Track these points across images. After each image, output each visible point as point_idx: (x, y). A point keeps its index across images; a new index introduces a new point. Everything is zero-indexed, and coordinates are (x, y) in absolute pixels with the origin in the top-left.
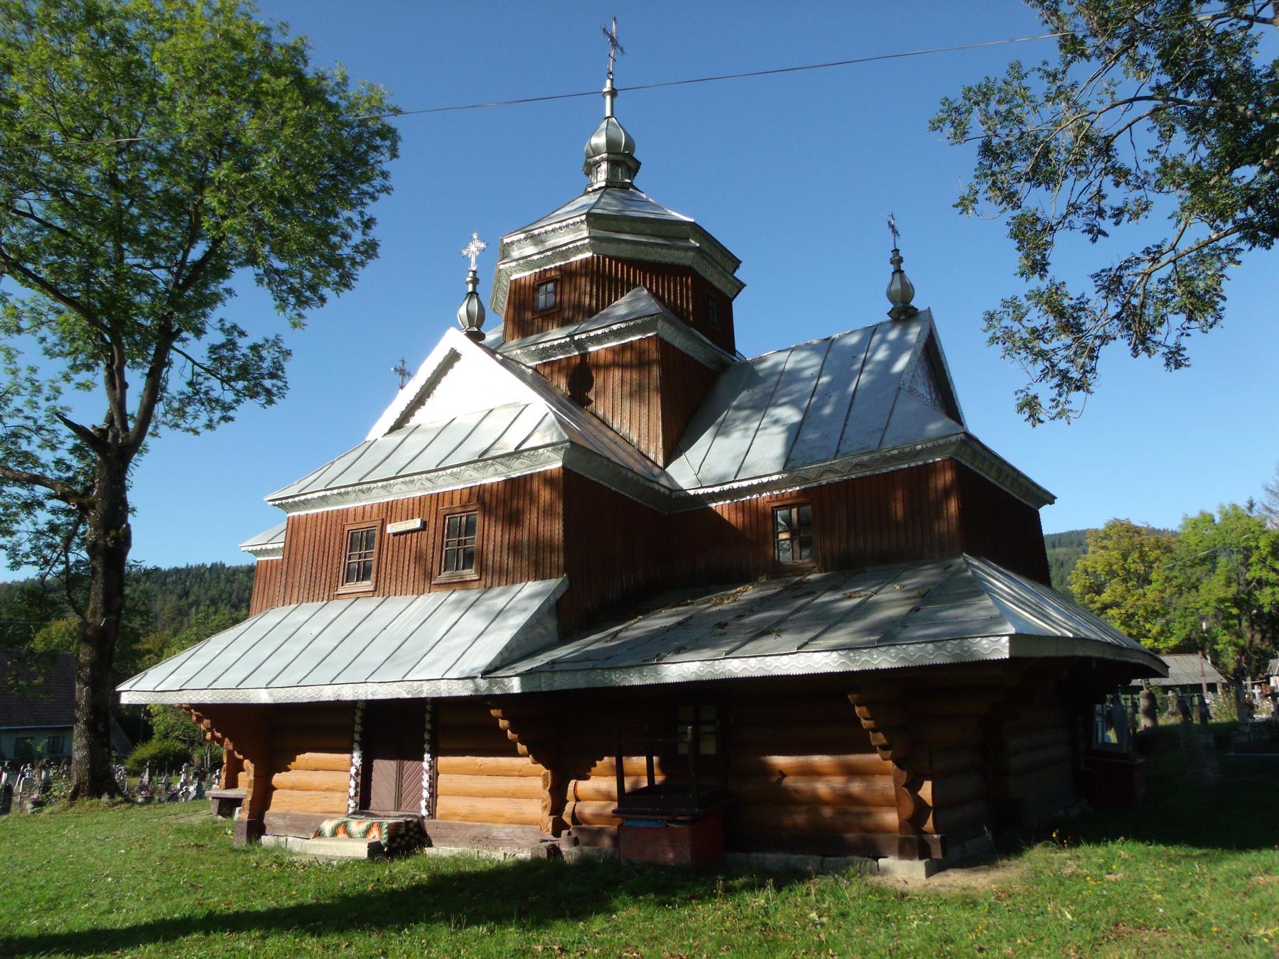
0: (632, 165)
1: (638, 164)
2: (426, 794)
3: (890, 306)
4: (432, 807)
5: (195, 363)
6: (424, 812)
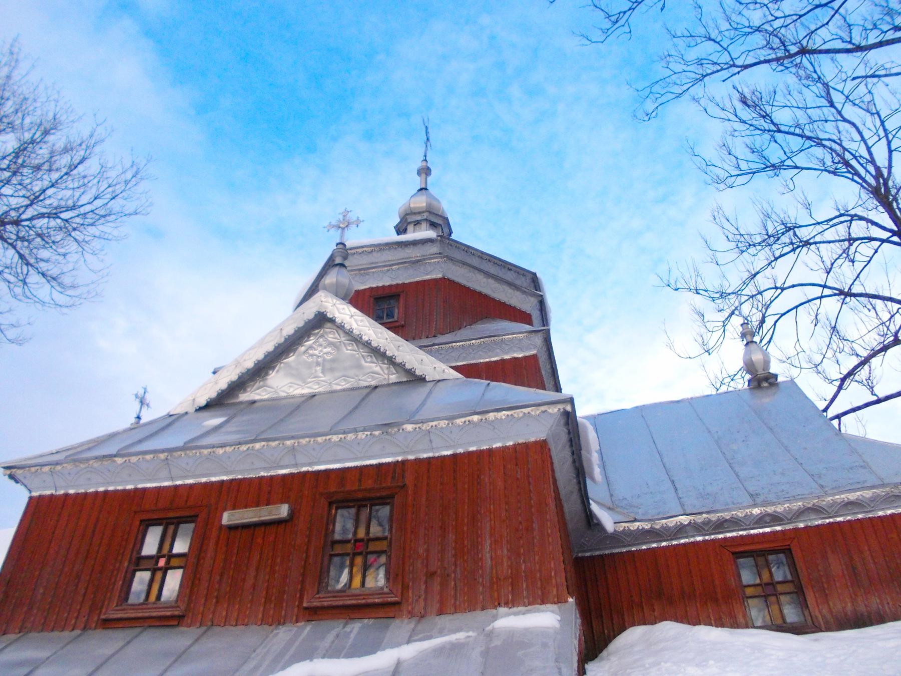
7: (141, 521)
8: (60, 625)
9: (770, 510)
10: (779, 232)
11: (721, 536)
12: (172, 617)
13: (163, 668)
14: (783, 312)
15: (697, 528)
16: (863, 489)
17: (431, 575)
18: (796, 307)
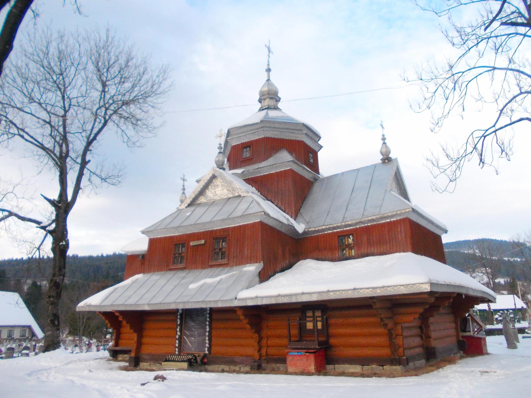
0: (278, 99)
1: (280, 99)
2: (207, 345)
3: (381, 157)
4: (210, 349)
5: (91, 172)
6: (207, 352)
7: (174, 244)
8: (161, 270)
9: (347, 223)
10: (470, 34)
11: (335, 231)
12: (183, 268)
13: (179, 281)
14: (470, 80)
15: (329, 229)
16: (373, 216)
17: (234, 257)
18: (476, 77)
